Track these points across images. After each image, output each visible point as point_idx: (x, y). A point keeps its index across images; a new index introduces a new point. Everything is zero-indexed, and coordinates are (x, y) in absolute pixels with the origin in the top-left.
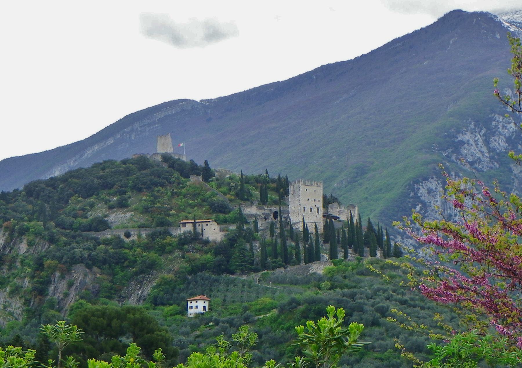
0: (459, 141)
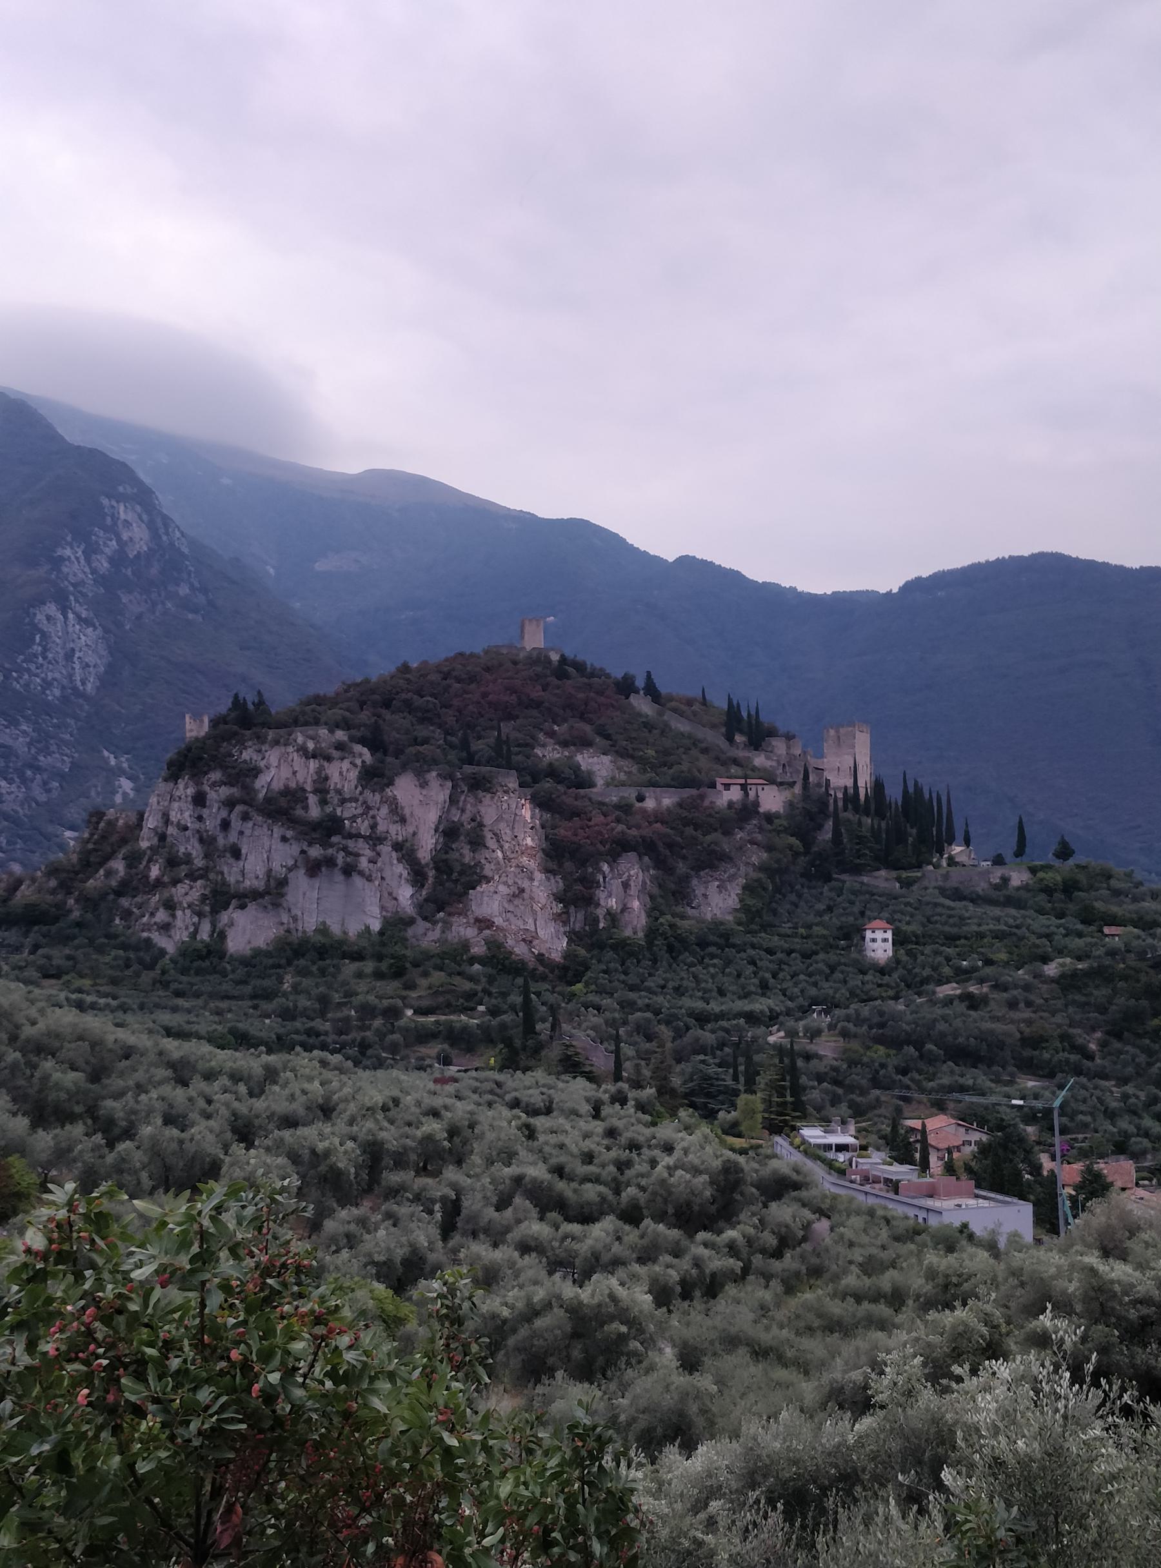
0: (641, 808)
